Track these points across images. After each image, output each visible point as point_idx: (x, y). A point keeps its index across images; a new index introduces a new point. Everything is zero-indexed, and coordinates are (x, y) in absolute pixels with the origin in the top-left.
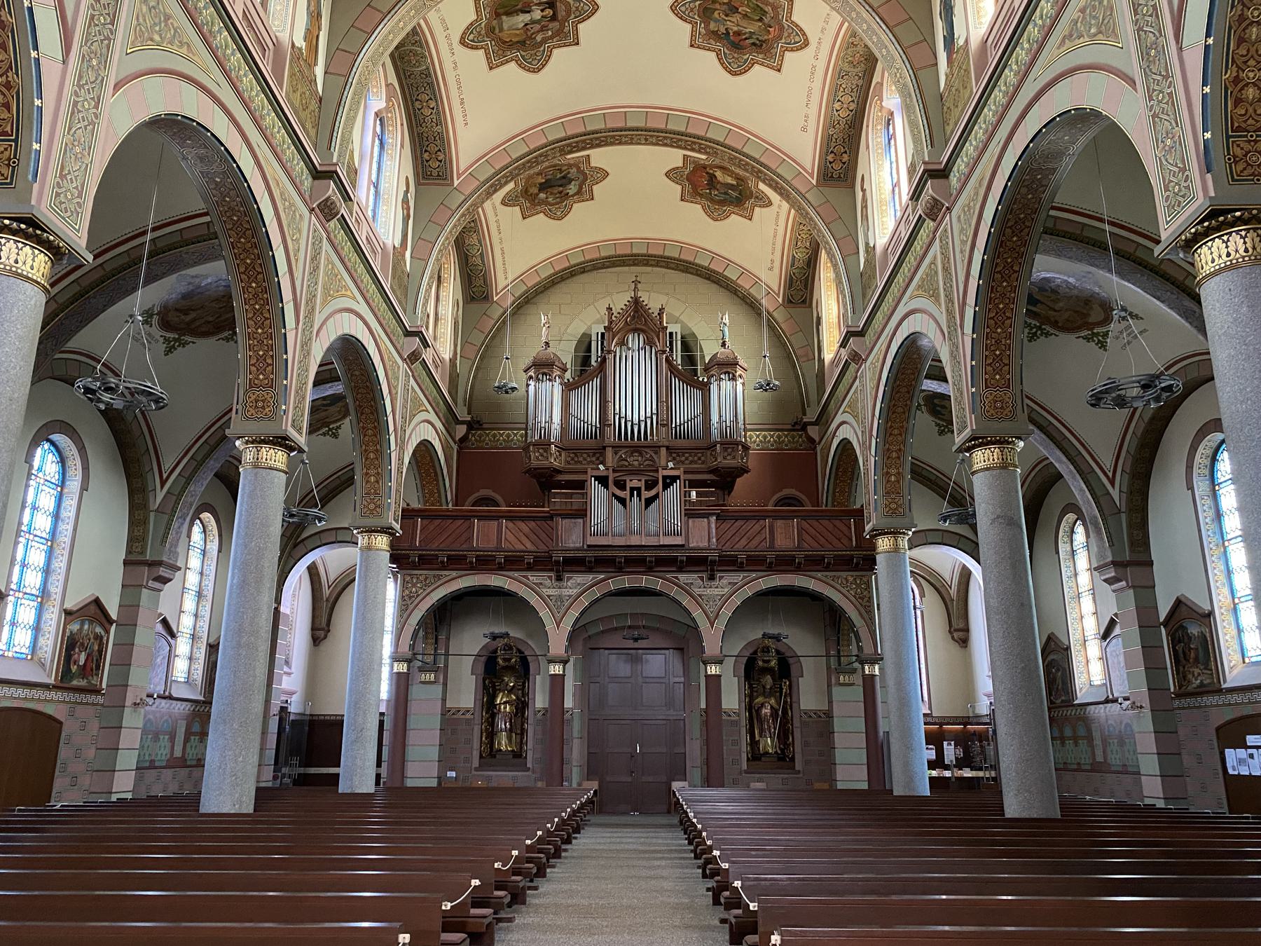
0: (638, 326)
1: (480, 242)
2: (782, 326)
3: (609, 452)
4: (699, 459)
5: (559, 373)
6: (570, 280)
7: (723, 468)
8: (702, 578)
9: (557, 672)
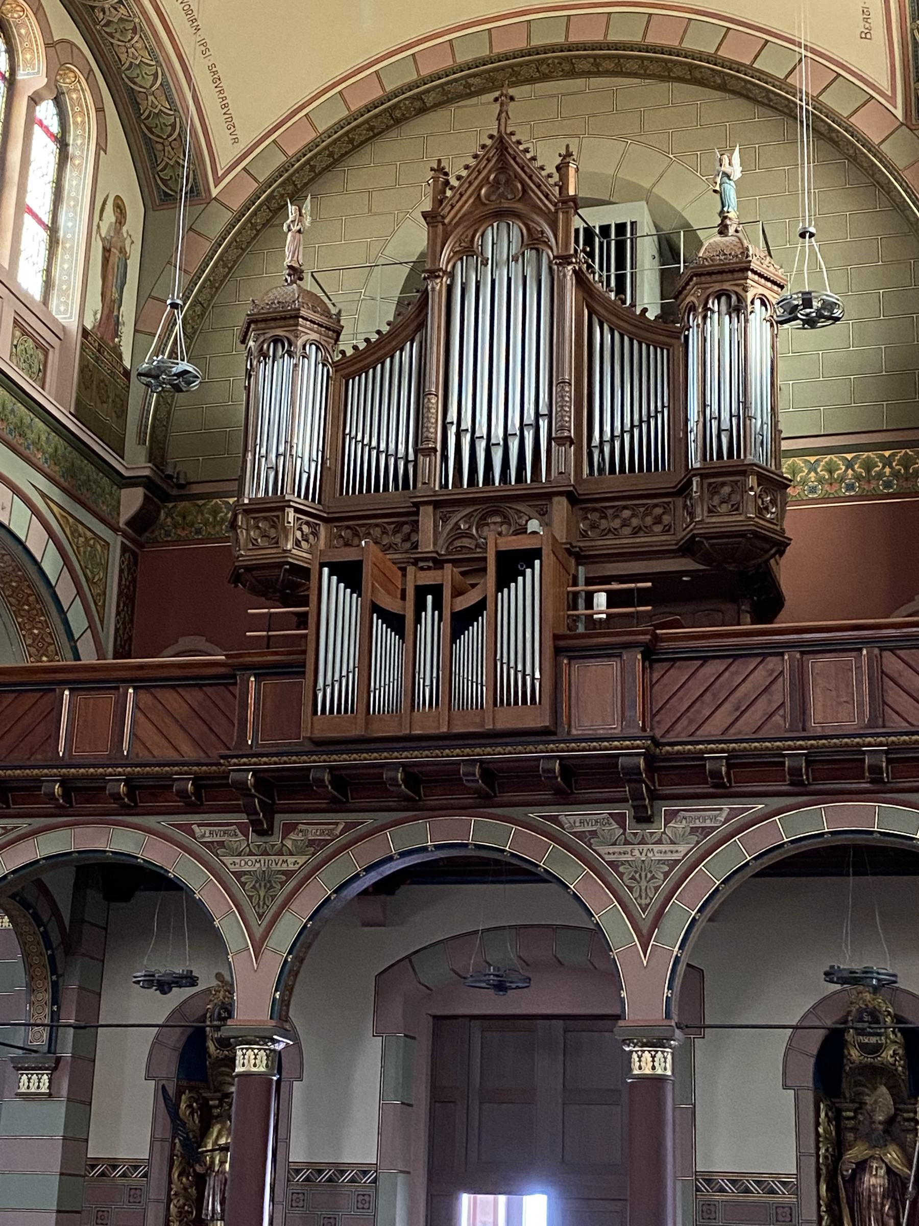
0: (506, 205)
1: (151, 52)
2: (908, 176)
3: (427, 519)
4: (658, 520)
5: (315, 336)
6: (393, 133)
7: (708, 537)
8: (620, 820)
9: (659, 1071)
